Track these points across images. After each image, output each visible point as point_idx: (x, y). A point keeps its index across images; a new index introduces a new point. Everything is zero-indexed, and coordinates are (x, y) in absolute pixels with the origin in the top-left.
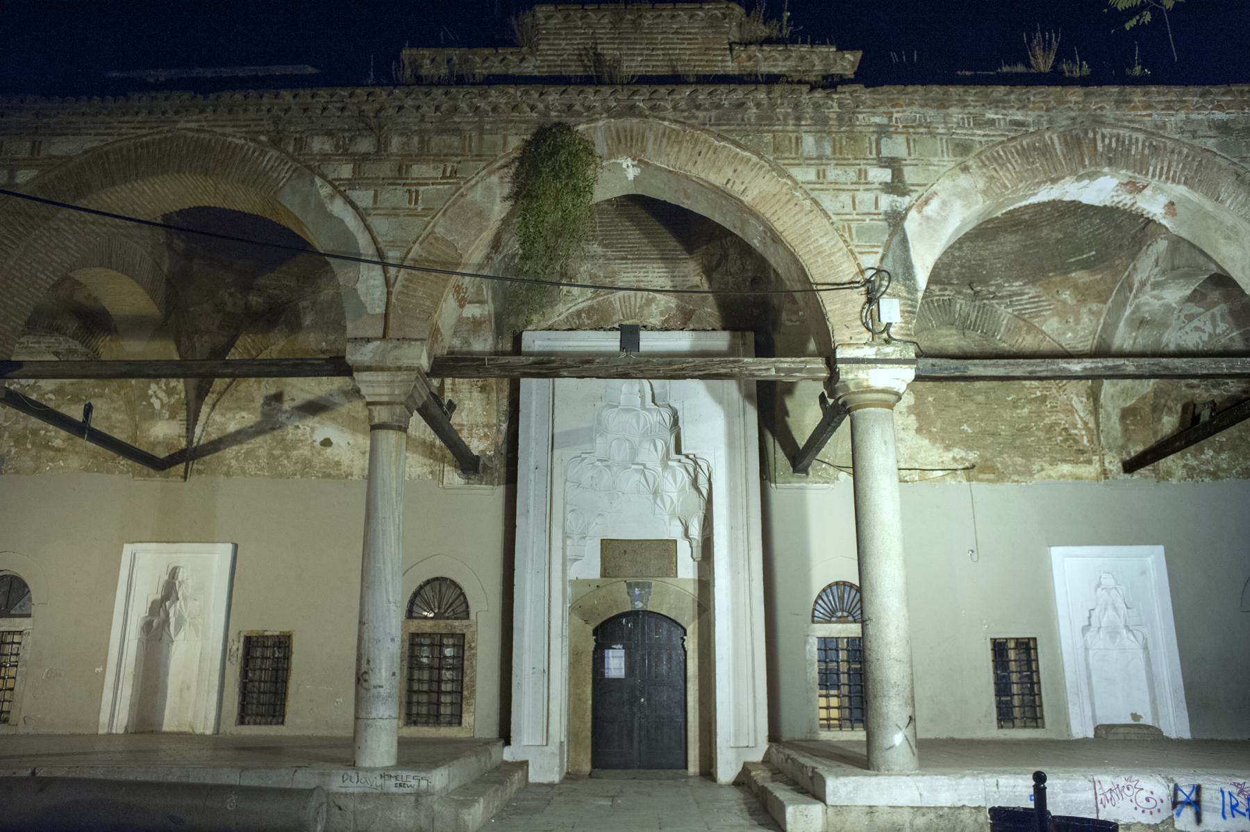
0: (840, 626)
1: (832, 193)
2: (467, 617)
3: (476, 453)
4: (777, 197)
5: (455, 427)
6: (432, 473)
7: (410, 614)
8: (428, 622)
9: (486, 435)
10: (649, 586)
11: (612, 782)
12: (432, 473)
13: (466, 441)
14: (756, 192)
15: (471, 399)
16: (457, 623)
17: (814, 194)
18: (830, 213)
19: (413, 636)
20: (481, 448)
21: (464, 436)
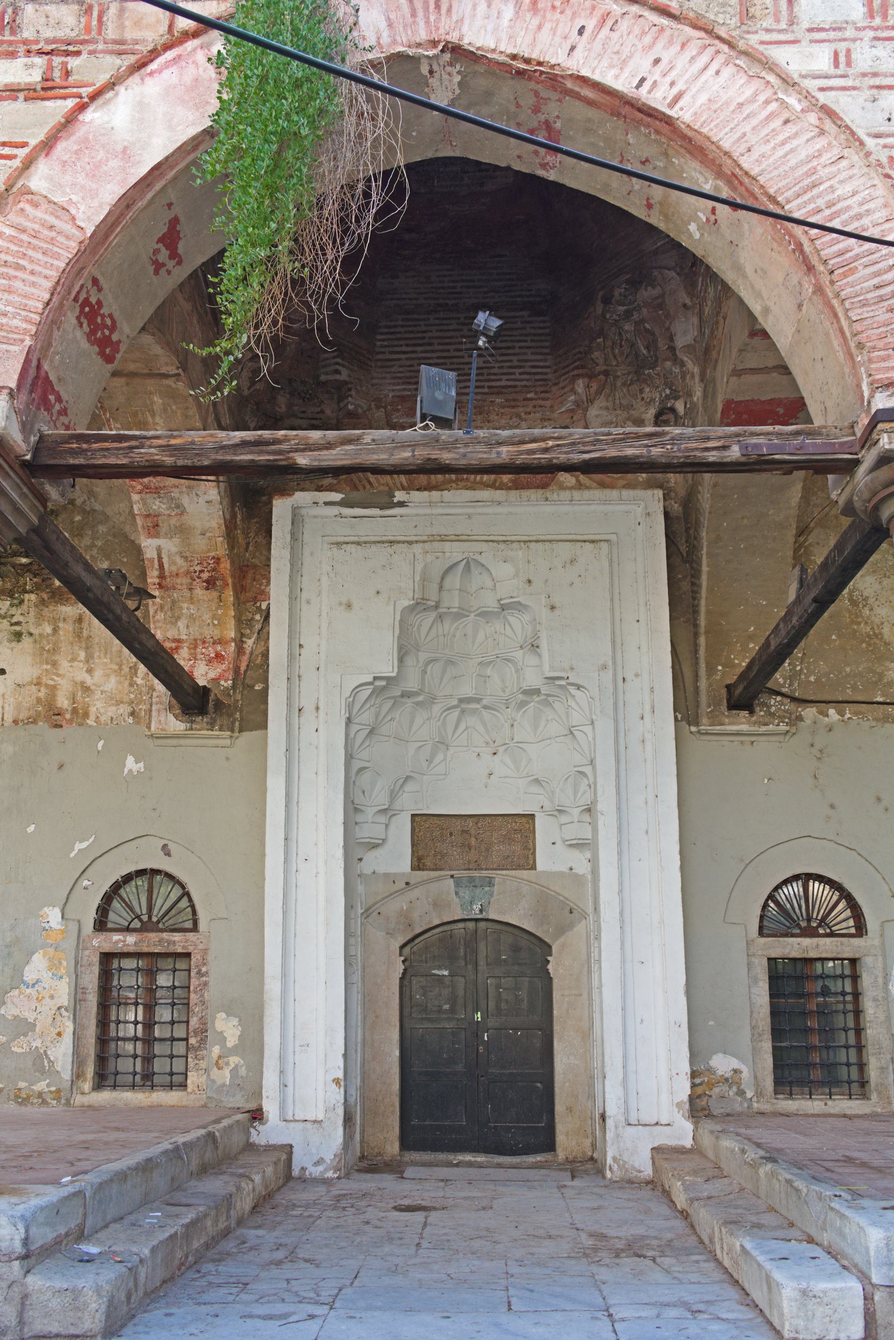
0: (807, 941)
1: (868, 93)
2: (195, 929)
3: (201, 682)
4: (747, 110)
5: (168, 645)
6: (132, 714)
7: (101, 925)
8: (443, 899)
9: (218, 656)
10: (490, 882)
11: (430, 1179)
12: (132, 714)
13: (186, 665)
14: (703, 98)
15: (191, 600)
16: (177, 937)
17: (822, 98)
18: (861, 133)
19: (107, 958)
20: (212, 675)
21: (183, 658)
